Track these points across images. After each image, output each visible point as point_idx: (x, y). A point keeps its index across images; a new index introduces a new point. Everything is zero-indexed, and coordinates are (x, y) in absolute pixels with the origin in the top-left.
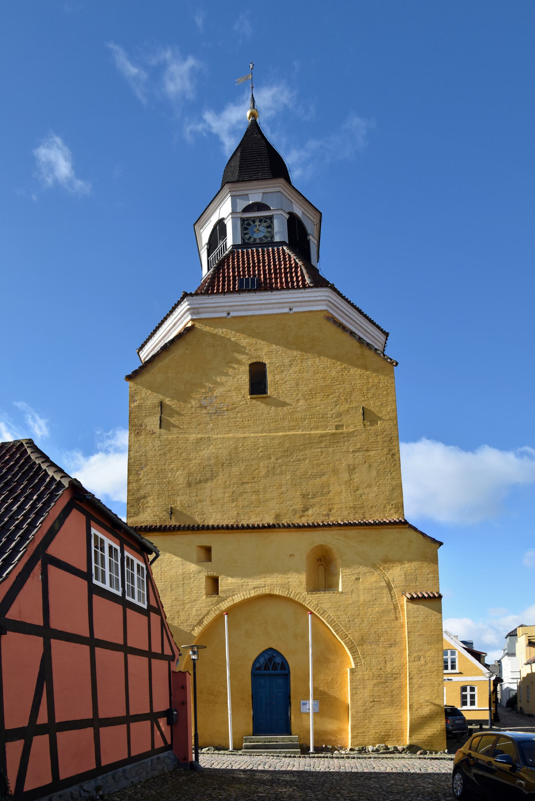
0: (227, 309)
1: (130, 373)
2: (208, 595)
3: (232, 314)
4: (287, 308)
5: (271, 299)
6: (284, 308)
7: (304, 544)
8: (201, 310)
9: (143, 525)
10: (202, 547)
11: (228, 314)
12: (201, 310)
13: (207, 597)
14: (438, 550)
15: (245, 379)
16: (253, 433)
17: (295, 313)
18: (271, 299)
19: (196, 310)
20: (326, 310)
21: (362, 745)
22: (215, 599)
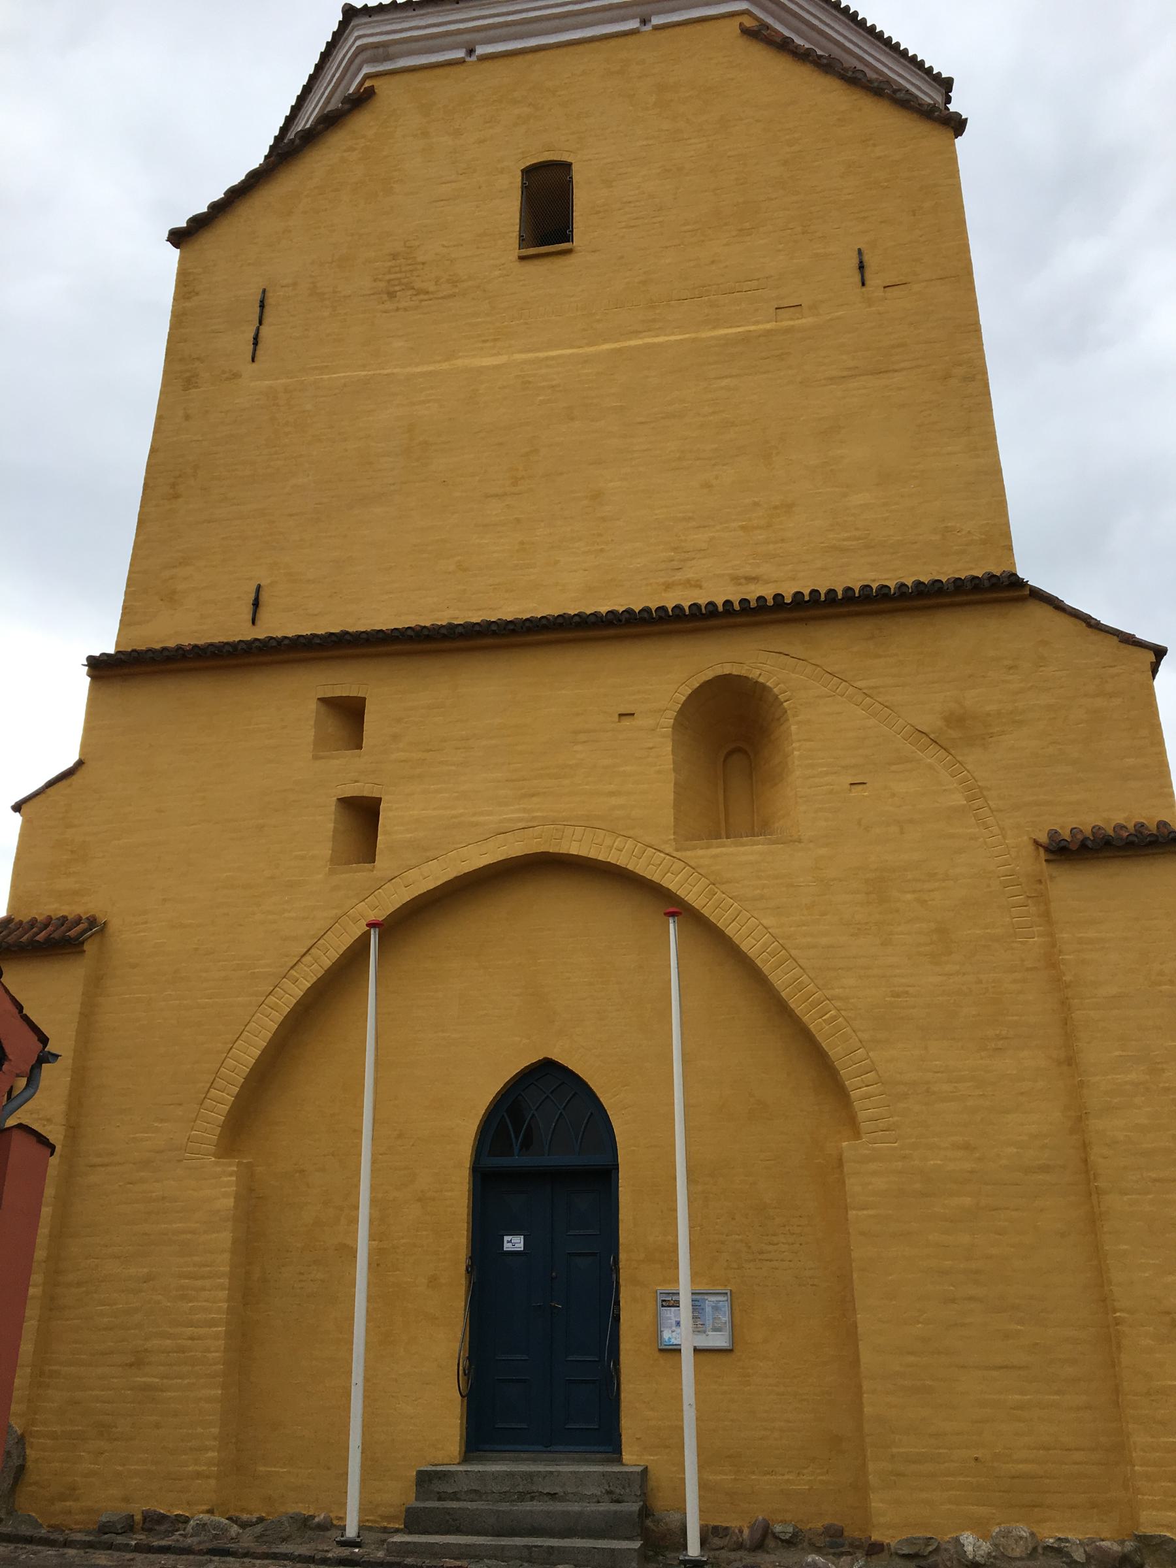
0: (467, 37)
1: (183, 224)
2: (338, 861)
3: (480, 50)
4: (633, 17)
5: (832, 28)
6: (624, 19)
7: (666, 679)
8: (392, 50)
9: (171, 644)
10: (323, 700)
11: (471, 52)
12: (392, 50)
13: (332, 872)
14: (1156, 683)
15: (507, 211)
16: (521, 352)
17: (657, 28)
18: (832, 28)
19: (381, 50)
20: (746, 12)
21: (73, 1130)
22: (360, 875)
